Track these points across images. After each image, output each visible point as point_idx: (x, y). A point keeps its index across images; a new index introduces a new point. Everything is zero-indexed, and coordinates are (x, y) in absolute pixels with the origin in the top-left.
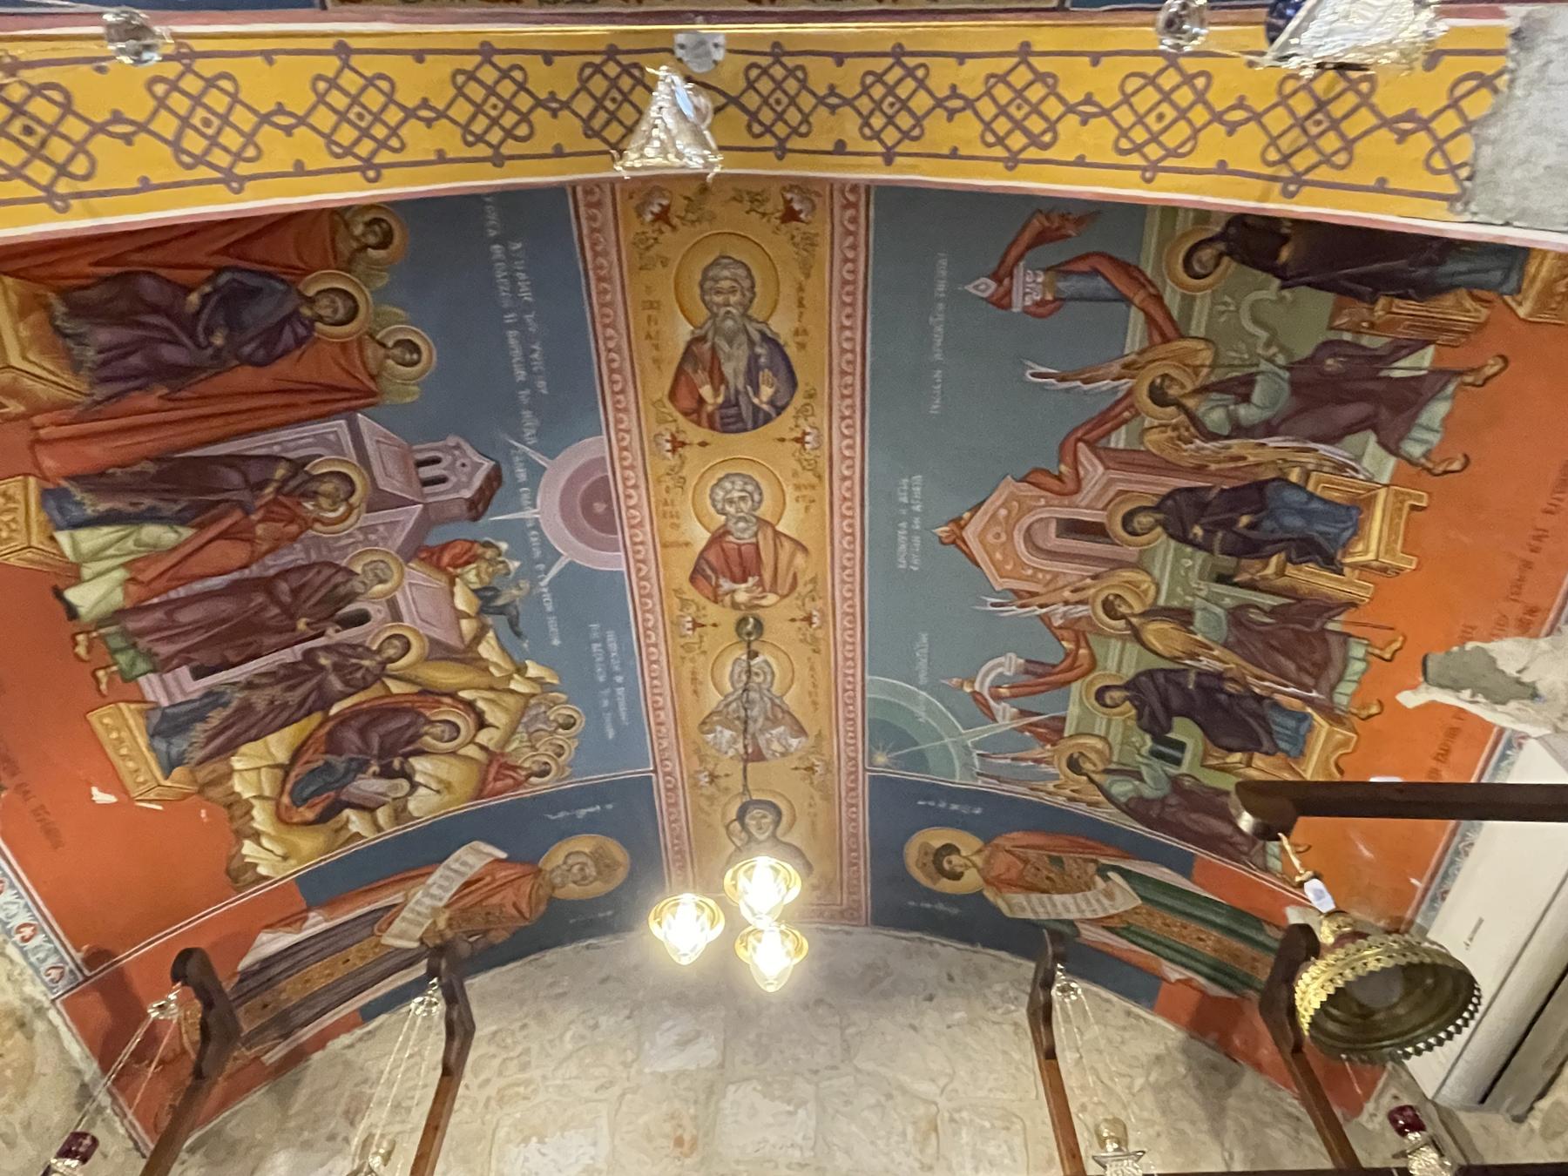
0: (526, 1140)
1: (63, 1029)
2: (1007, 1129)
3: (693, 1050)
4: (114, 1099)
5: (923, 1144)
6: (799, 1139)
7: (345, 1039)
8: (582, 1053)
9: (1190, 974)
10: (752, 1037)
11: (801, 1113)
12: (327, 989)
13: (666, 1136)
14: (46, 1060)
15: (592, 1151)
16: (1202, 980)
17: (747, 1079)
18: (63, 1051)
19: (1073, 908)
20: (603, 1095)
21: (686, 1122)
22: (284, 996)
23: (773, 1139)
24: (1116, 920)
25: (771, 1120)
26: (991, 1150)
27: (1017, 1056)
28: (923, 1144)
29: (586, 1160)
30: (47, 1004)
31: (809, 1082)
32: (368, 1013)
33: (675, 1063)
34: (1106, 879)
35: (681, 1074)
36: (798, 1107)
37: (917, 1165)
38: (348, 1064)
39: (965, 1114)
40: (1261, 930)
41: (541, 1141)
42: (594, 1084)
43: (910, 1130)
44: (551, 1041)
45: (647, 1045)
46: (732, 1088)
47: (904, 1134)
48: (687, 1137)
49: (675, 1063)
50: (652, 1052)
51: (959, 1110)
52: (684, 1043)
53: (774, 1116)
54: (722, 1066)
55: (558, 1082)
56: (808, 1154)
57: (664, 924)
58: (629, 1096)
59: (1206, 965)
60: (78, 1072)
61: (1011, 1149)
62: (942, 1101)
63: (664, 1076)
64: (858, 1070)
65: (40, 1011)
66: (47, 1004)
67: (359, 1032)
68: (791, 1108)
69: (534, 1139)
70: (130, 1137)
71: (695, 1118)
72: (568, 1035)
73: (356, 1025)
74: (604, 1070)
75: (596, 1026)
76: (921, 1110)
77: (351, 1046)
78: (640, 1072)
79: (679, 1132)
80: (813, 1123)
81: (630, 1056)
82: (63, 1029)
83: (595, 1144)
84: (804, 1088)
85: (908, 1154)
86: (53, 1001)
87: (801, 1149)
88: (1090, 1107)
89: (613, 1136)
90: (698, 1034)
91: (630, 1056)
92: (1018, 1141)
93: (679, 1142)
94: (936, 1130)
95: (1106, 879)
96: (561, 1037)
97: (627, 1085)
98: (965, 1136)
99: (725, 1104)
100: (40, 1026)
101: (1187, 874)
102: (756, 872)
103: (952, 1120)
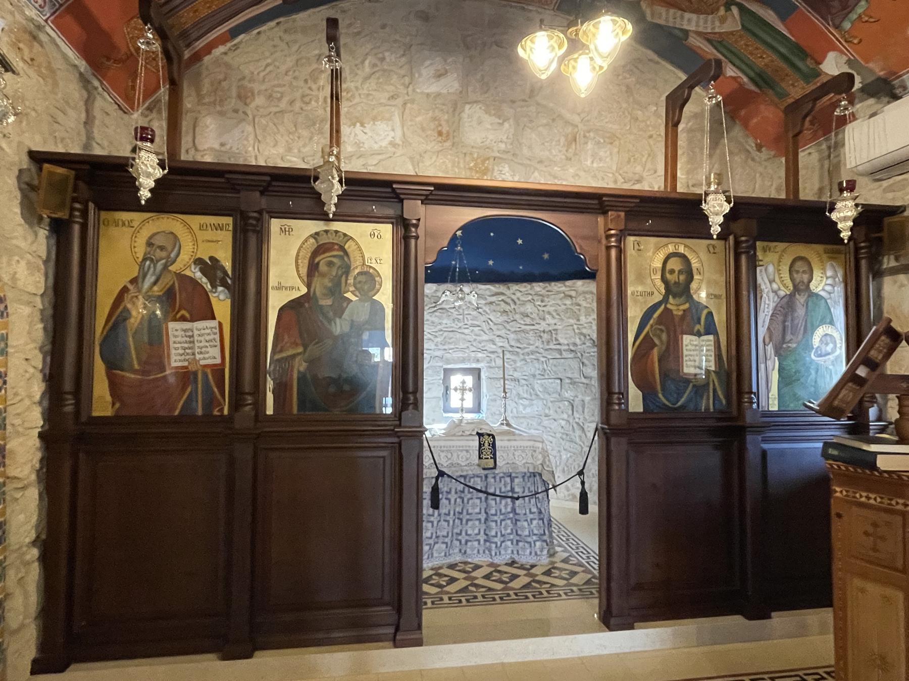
0: (354, 125)
1: (58, 40)
2: (611, 143)
3: (443, 81)
4: (102, 83)
5: (569, 145)
6: (504, 138)
7: (221, 49)
8: (377, 75)
9: (740, 74)
10: (478, 76)
11: (506, 125)
12: (208, 17)
13: (434, 130)
14: (58, 64)
15: (392, 134)
16: (745, 79)
17: (476, 102)
18: (65, 57)
19: (694, 23)
20: (392, 102)
21: (443, 123)
22: (183, 20)
23: (491, 137)
24: (717, 36)
25: (489, 127)
26: (602, 153)
27: (624, 105)
28: (569, 145)
29: (390, 138)
30: (43, 23)
31: (511, 108)
32: (234, 33)
33: (433, 89)
34: (728, 9)
35: (438, 95)
36: (504, 121)
37: (564, 157)
38: (228, 66)
39: (592, 134)
40: (803, 60)
41: (362, 125)
42: (387, 95)
43: (563, 139)
44: (356, 65)
45: (417, 75)
46: (467, 107)
47: (559, 141)
48: (444, 131)
49: (433, 89)
50: (420, 79)
51: (589, 132)
52: (439, 76)
53: (491, 124)
54: (461, 92)
55: (365, 92)
56: (509, 147)
57: (528, 49)
58: (409, 105)
59: (753, 70)
60: (75, 66)
61: (611, 154)
62: (581, 126)
63: (428, 95)
64: (538, 104)
65: (39, 27)
66: (43, 23)
67: (229, 45)
68: (501, 121)
69: (358, 124)
70: (116, 103)
71: (447, 121)
72: (367, 62)
73: (227, 41)
74: (393, 88)
75: (383, 59)
76: (569, 129)
77: (225, 53)
78: (414, 90)
79: (440, 129)
80: (512, 131)
81: (407, 80)
82: (58, 40)
83: (393, 130)
84: (507, 110)
85: (560, 151)
86: (46, 21)
87: (506, 143)
88: (655, 136)
89: (403, 127)
90: (446, 72)
91: (407, 80)
92: (616, 150)
93: (440, 134)
94: (575, 140)
95: (728, 9)
96: (363, 62)
97: (407, 98)
98: (590, 146)
99: (464, 116)
100: (43, 37)
101: (783, 18)
102: (601, 26)
103: (585, 136)
